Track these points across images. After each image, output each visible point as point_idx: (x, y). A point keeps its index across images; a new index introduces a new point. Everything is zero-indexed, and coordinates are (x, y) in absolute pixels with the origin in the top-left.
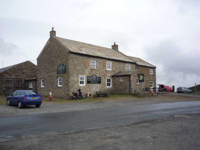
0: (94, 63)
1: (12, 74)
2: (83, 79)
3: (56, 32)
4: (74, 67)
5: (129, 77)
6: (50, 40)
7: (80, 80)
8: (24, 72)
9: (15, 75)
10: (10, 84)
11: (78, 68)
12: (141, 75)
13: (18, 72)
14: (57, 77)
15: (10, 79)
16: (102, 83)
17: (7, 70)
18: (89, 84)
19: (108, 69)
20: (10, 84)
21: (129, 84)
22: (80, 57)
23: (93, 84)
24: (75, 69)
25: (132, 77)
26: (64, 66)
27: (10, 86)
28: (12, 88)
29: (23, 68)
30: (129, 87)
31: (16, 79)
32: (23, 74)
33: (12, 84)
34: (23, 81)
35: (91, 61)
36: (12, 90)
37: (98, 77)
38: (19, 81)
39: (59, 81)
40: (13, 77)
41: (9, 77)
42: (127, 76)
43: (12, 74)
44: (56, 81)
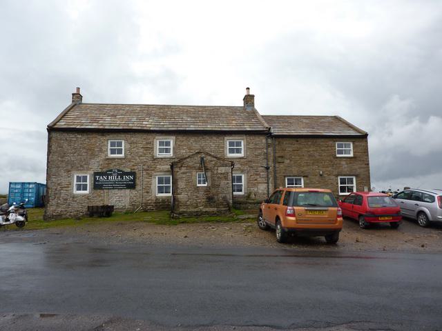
0: (120, 144)
4: (62, 158)
7: (340, 185)
16: (138, 187)
23: (110, 191)
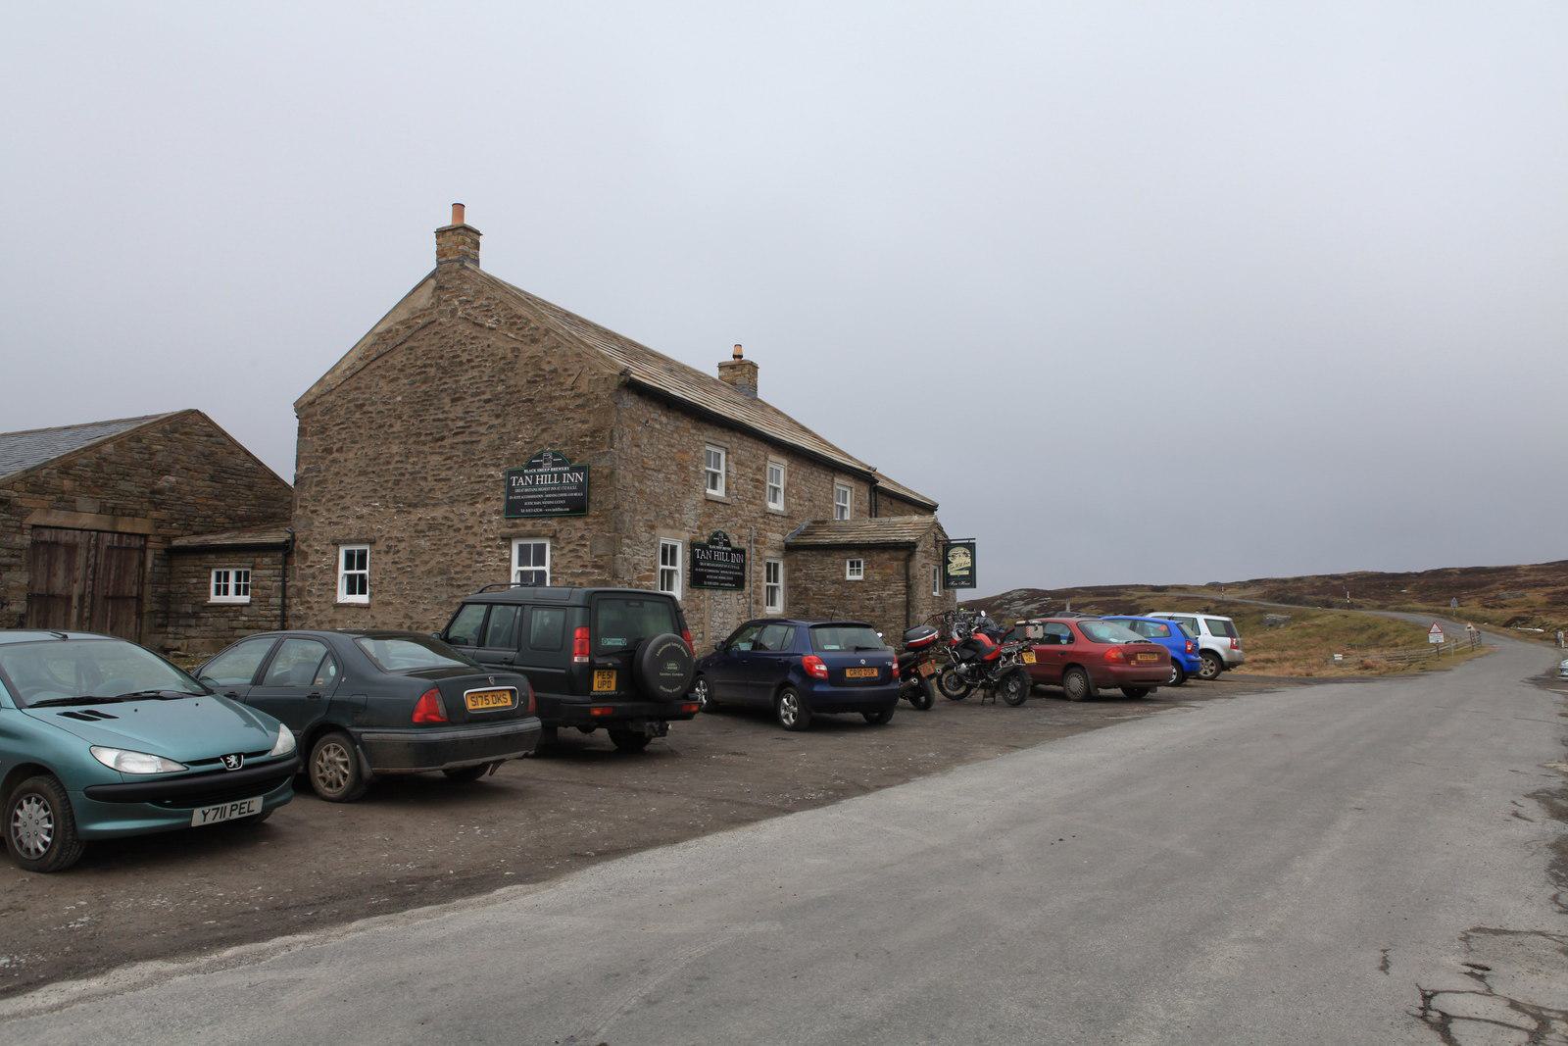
1: (83, 502)
3: (482, 240)
4: (640, 482)
5: (902, 555)
6: (440, 288)
8: (160, 492)
9: (102, 510)
10: (61, 573)
11: (655, 485)
12: (960, 550)
13: (123, 485)
14: (508, 539)
15: (64, 537)
17: (43, 466)
18: (697, 593)
19: (772, 506)
20: (61, 573)
21: (901, 598)
22: (664, 419)
24: (641, 492)
25: (919, 559)
26: (578, 469)
27: (59, 583)
28: (75, 601)
29: (159, 457)
30: (899, 613)
31: (108, 537)
32: (157, 506)
33: (79, 574)
34: (150, 555)
36: (75, 612)
38: (128, 549)
39: (342, 571)
40: (87, 520)
41: (58, 518)
42: (894, 554)
43: (83, 502)
44: (493, 562)
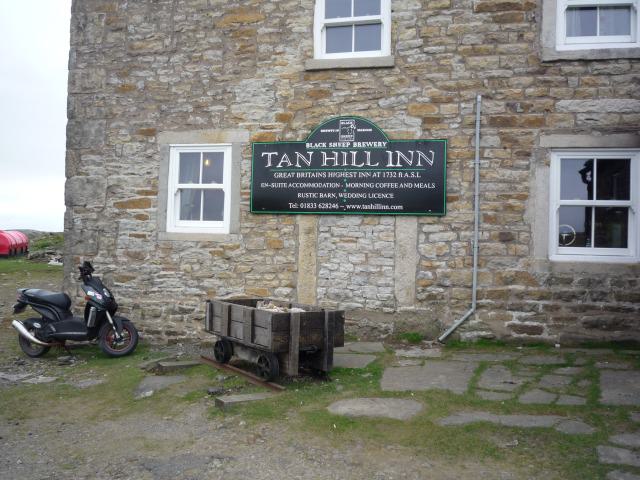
2: (215, 174)
4: (122, 75)
16: (458, 211)
18: (272, 221)
35: (384, 52)
37: (394, 145)
